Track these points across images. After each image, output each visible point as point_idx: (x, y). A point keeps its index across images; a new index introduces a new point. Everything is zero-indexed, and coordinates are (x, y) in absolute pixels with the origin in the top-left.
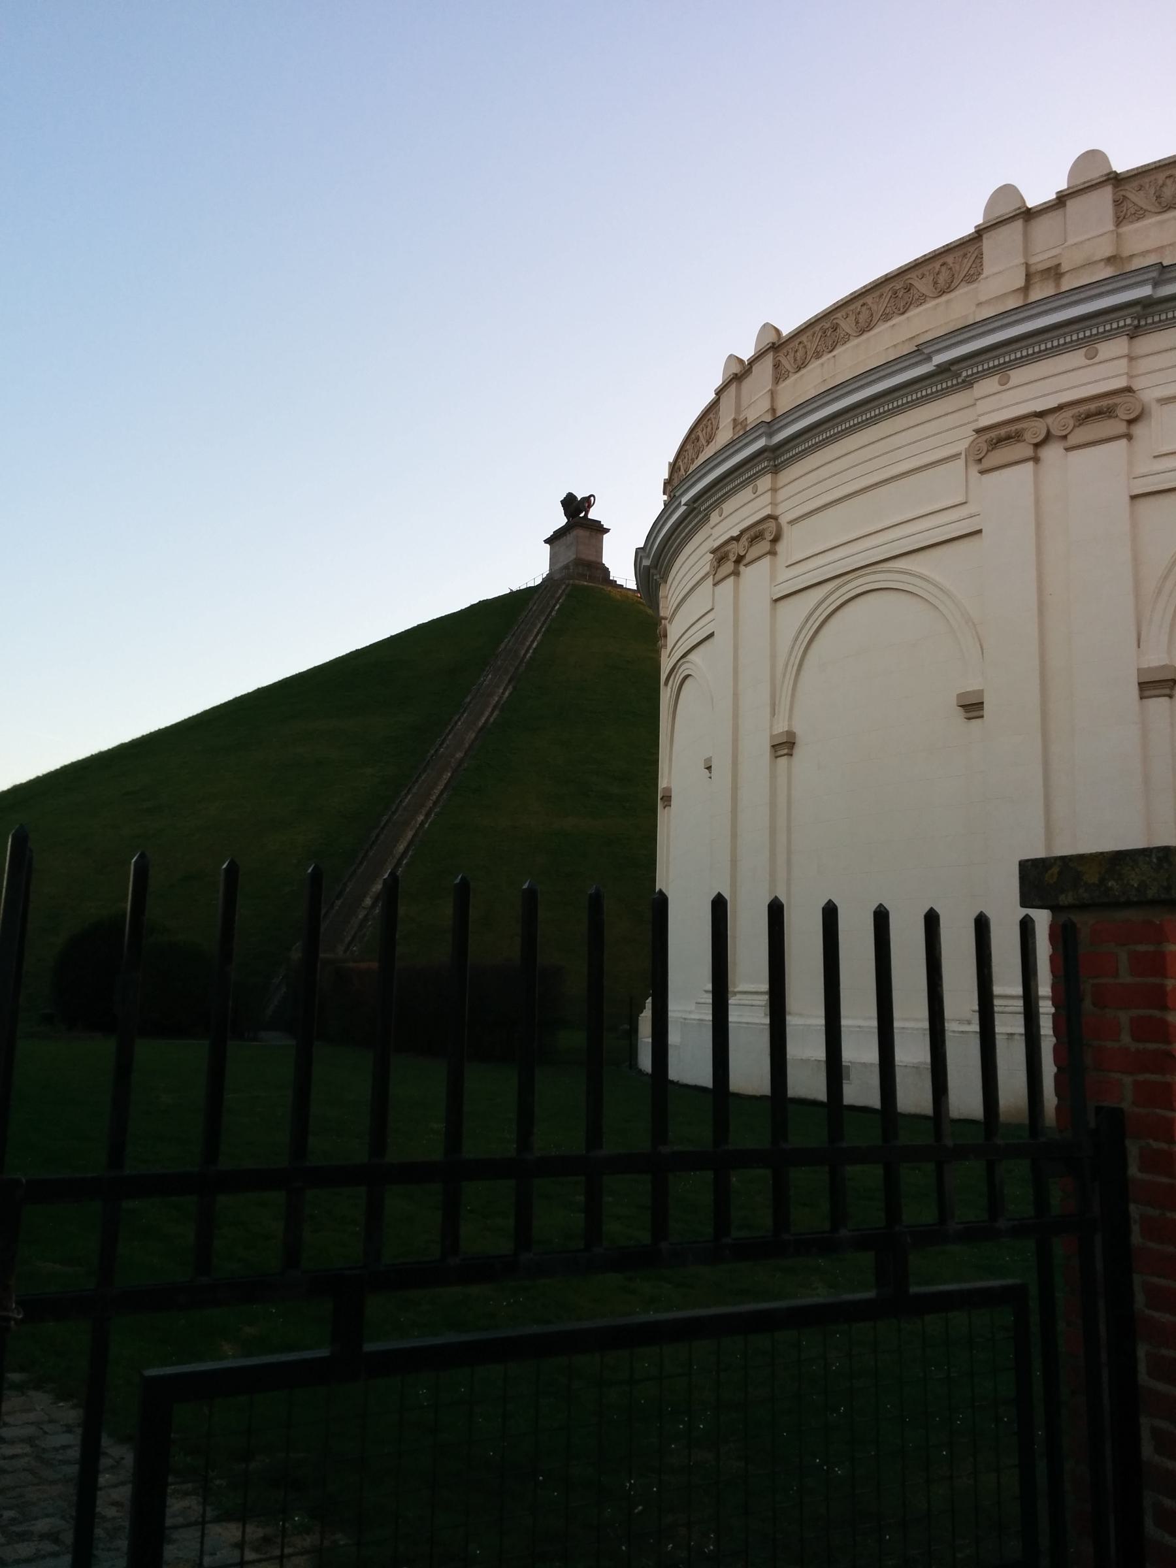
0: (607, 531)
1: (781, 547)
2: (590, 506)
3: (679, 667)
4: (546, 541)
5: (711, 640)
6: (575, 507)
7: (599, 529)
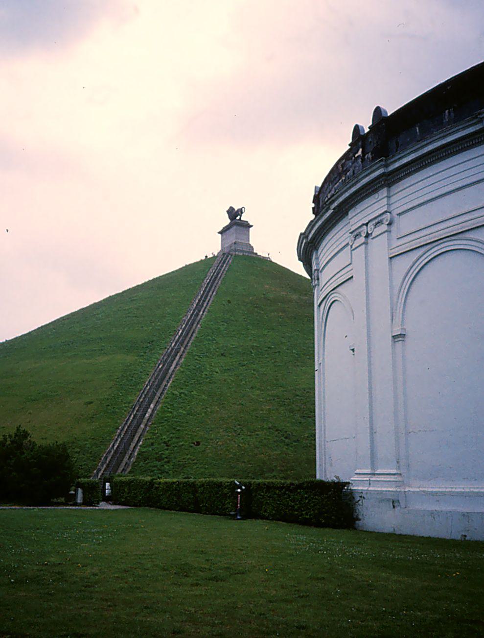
0: (252, 226)
1: (394, 228)
2: (242, 213)
3: (331, 295)
4: (219, 233)
5: (351, 280)
6: (234, 214)
7: (248, 226)
